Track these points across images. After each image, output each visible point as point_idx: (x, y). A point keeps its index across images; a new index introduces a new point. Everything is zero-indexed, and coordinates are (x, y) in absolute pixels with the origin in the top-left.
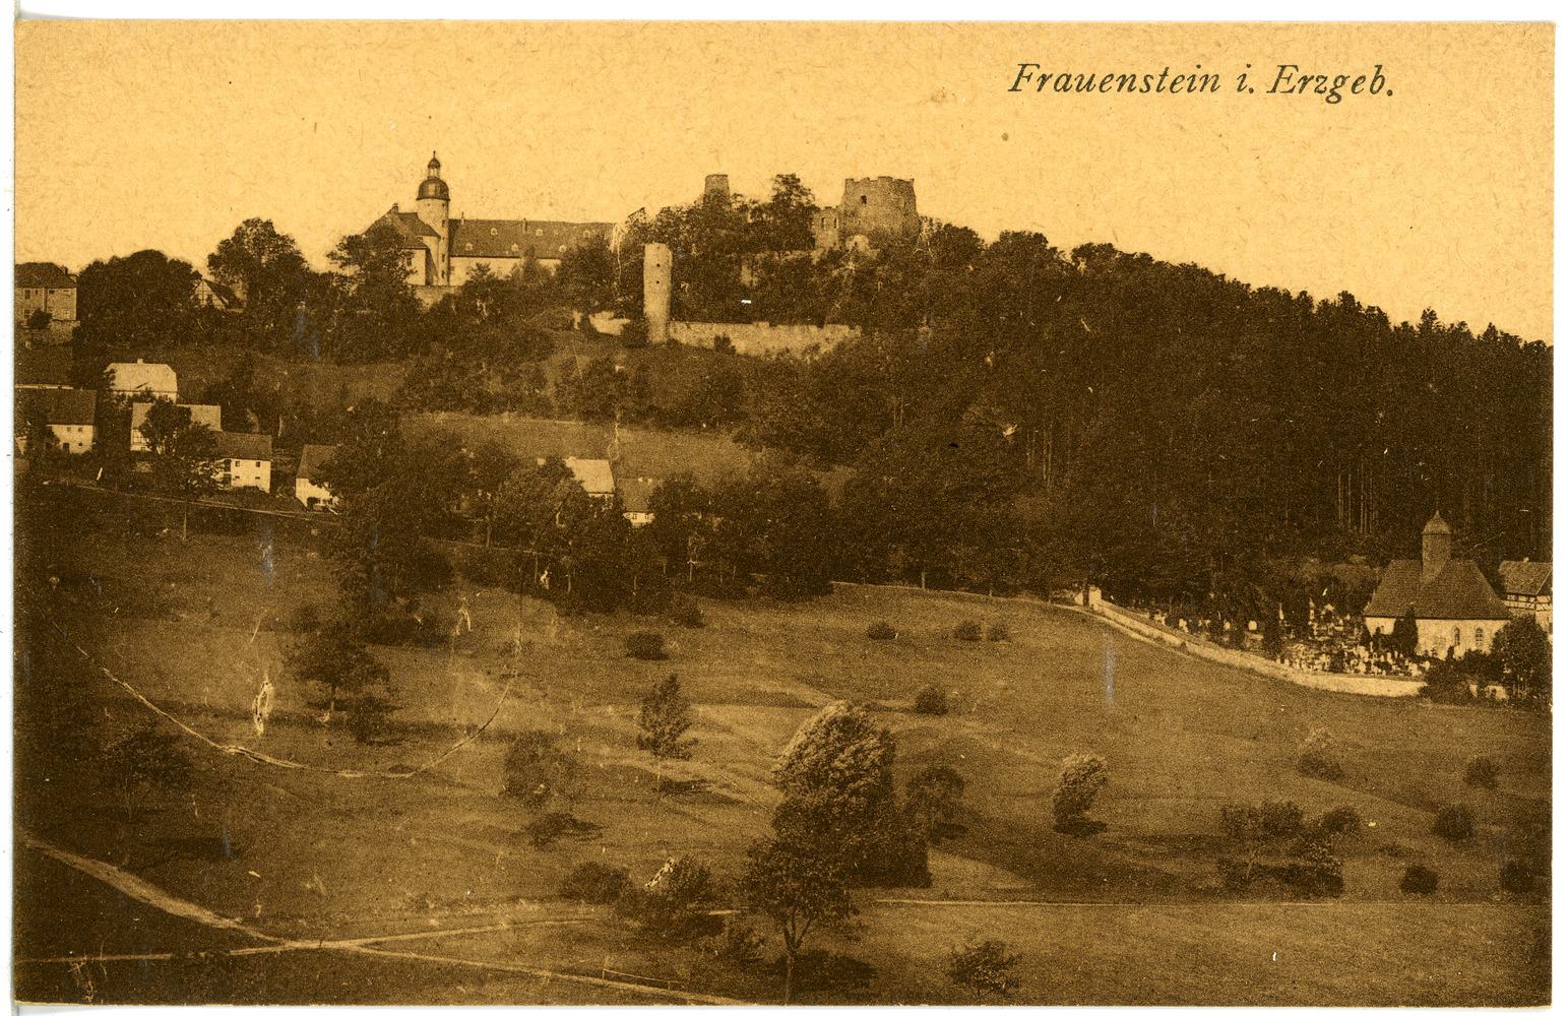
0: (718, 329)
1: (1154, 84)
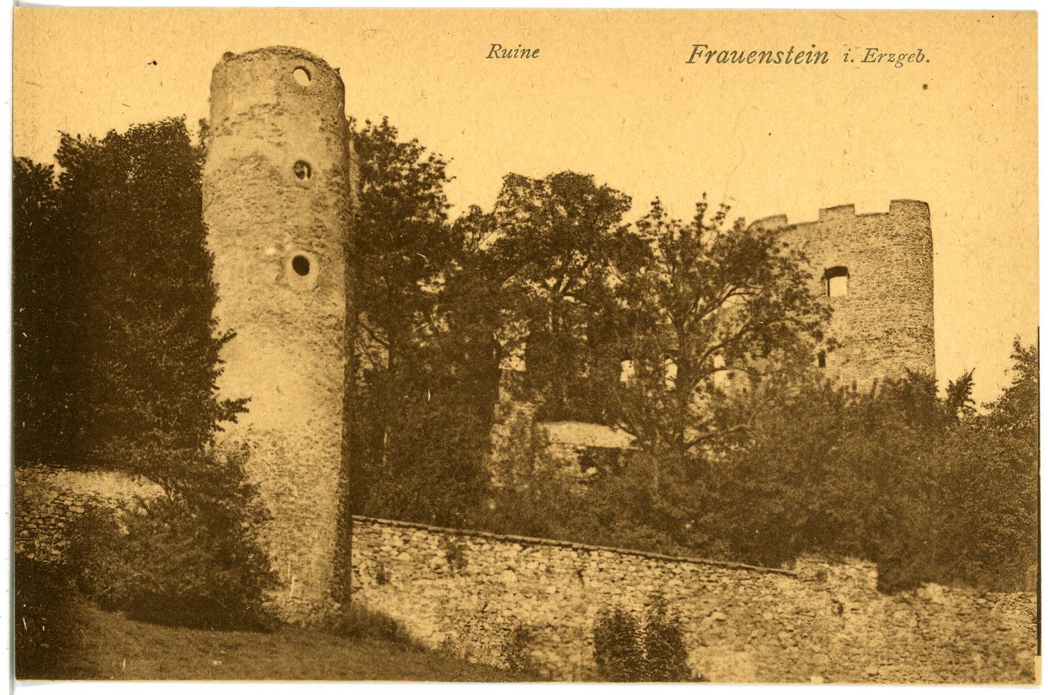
1: (784, 58)
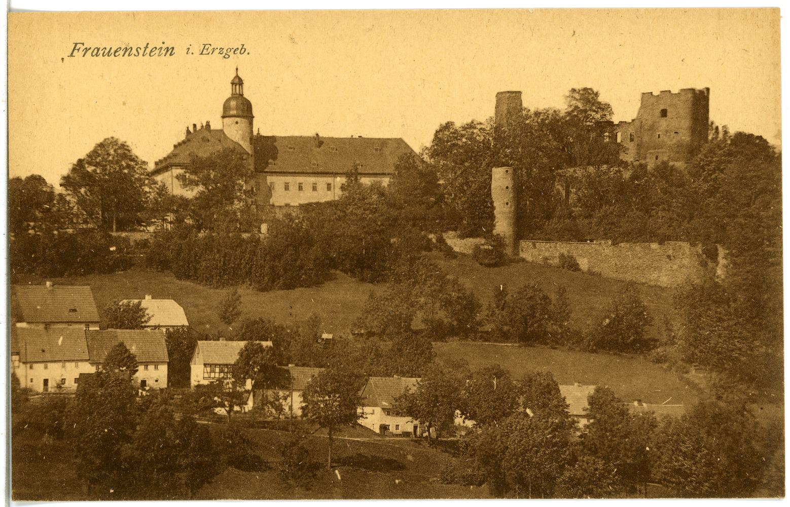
0: (562, 248)
1: (141, 52)
